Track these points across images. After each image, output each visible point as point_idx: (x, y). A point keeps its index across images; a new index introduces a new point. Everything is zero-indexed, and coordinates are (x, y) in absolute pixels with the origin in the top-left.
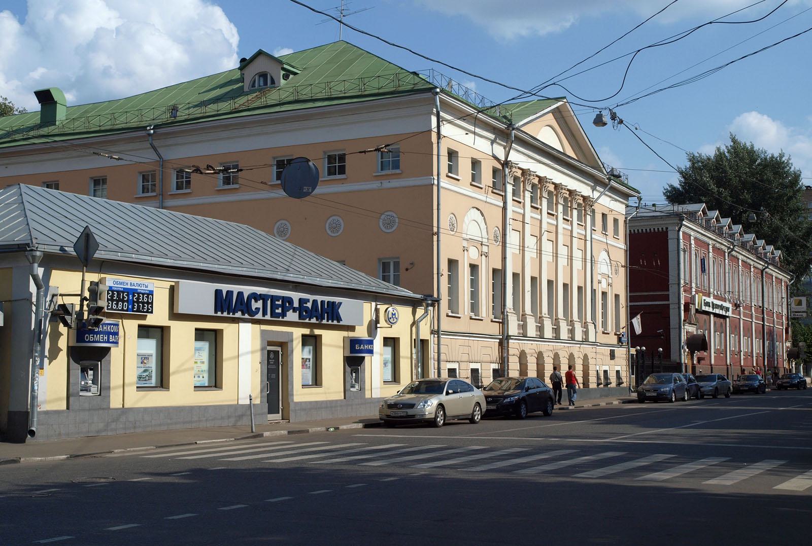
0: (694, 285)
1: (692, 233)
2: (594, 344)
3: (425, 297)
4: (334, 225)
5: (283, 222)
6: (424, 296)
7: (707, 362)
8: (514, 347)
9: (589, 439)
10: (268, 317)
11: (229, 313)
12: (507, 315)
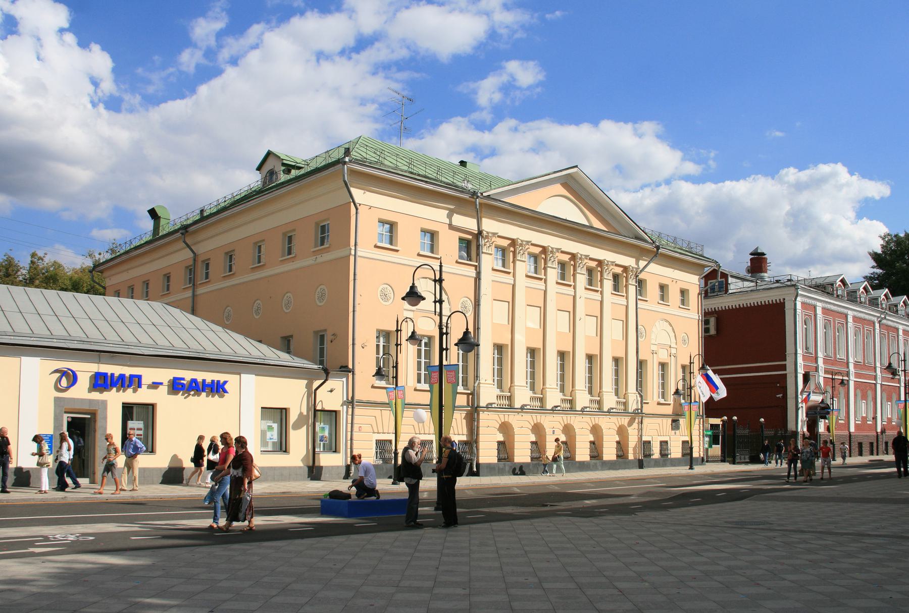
9: (471, 511)
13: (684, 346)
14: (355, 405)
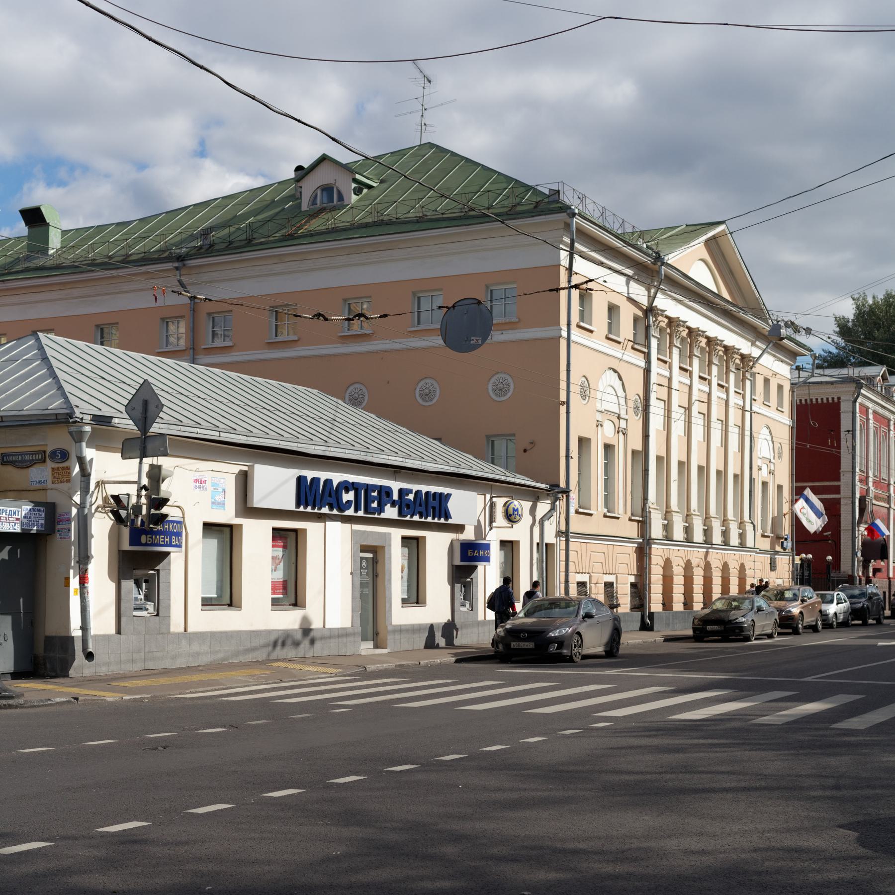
0: (871, 474)
1: (870, 405)
2: (753, 549)
3: (552, 487)
4: (427, 391)
5: (503, 376)
6: (550, 486)
7: (883, 574)
8: (658, 554)
10: (361, 513)
11: (313, 508)
12: (650, 512)
13: (636, 417)
14: (570, 537)
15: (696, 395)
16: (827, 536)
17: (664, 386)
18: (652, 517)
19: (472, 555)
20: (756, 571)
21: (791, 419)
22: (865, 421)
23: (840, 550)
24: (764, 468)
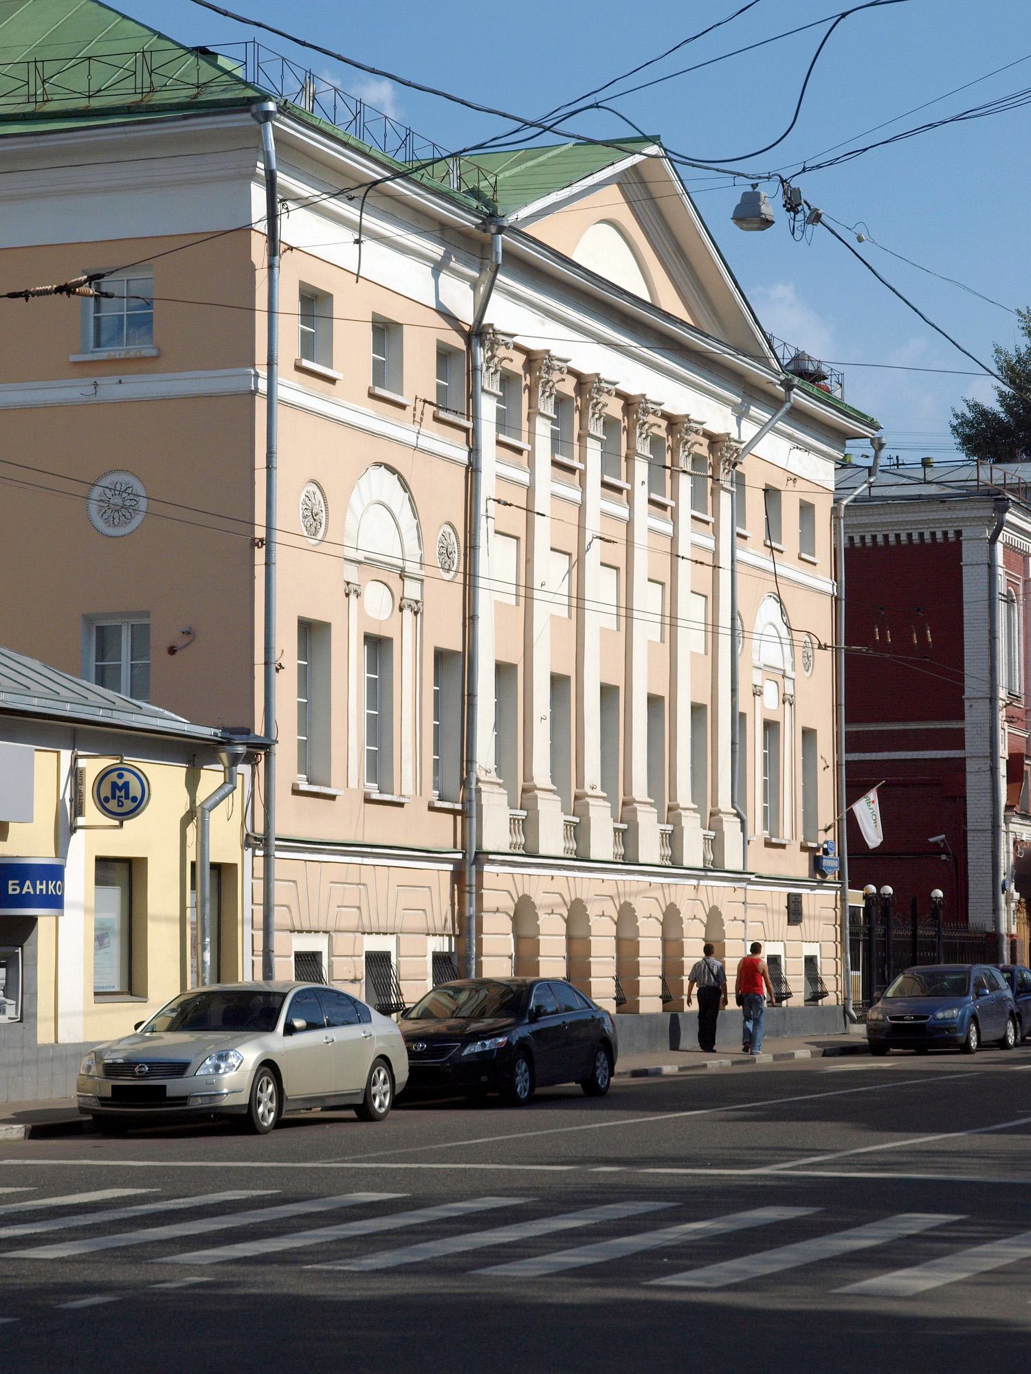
2: (741, 876)
6: (224, 730)
12: (479, 791)
15: (594, 524)
16: (936, 843)
17: (510, 505)
18: (483, 802)
19: (18, 892)
20: (749, 924)
21: (836, 580)
22: (1021, 584)
23: (966, 875)
24: (770, 691)
